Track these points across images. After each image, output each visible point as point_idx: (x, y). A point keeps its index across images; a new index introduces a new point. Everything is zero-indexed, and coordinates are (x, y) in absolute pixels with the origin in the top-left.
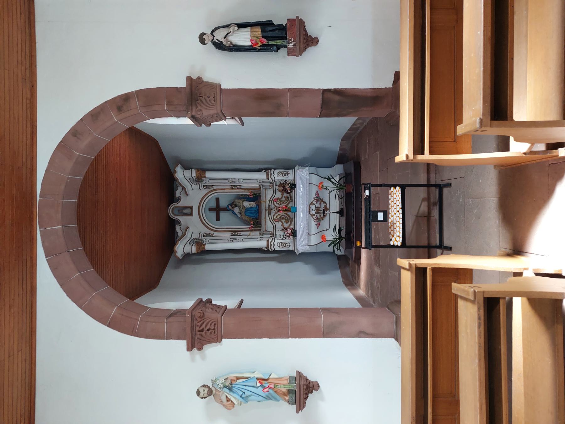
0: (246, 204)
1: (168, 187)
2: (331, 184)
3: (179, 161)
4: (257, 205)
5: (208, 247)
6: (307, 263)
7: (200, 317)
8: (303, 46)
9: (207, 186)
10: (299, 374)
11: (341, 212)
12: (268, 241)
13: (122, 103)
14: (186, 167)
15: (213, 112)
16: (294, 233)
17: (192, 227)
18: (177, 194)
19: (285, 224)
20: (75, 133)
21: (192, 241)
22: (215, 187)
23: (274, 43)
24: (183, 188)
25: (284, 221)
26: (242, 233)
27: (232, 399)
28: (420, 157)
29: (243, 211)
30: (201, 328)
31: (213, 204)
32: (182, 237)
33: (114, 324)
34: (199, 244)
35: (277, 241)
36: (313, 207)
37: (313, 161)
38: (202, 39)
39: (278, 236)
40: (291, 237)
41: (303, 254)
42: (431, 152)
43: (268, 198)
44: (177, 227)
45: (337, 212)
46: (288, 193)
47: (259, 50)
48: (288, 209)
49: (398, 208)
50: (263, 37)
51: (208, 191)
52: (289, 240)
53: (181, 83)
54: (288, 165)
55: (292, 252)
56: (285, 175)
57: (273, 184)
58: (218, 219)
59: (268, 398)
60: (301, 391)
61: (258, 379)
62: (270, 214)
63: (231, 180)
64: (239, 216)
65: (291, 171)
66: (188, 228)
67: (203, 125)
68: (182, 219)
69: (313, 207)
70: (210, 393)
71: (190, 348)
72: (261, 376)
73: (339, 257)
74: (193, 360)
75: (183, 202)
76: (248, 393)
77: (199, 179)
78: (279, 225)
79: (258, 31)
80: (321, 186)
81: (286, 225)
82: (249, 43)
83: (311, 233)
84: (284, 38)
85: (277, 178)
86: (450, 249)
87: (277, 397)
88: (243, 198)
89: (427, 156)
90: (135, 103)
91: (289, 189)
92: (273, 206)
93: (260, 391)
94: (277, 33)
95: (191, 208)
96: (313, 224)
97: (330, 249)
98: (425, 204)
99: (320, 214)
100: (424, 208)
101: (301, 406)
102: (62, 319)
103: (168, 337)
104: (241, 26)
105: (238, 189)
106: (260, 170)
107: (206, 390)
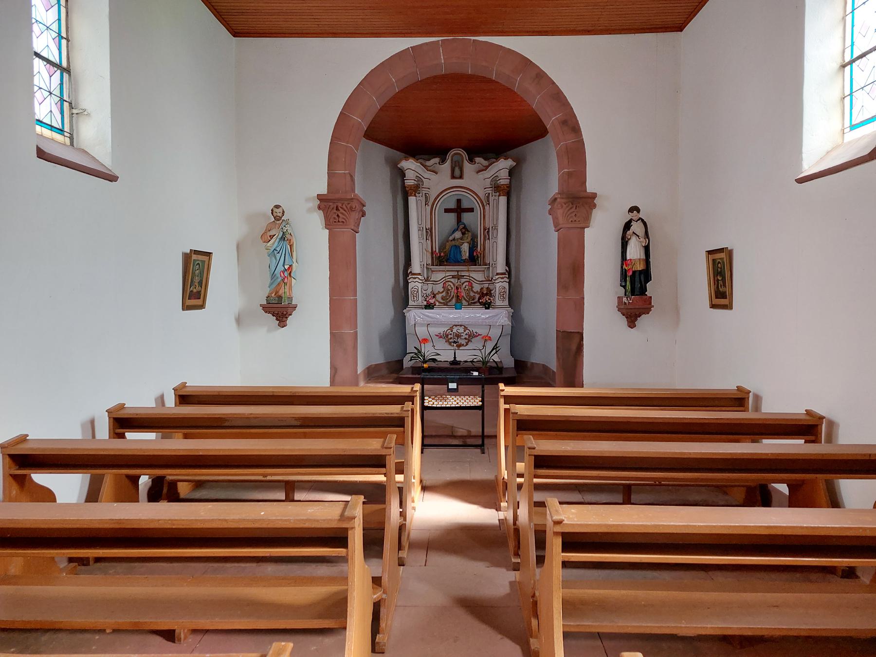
0: (465, 247)
1: (488, 147)
2: (488, 350)
3: (519, 162)
4: (465, 261)
5: (412, 200)
6: (393, 322)
7: (351, 208)
8: (624, 311)
9: (488, 197)
10: (295, 307)
11: (455, 362)
12: (419, 274)
13: (571, 125)
14: (511, 172)
15: (561, 220)
16: (429, 306)
17: (435, 178)
18: (478, 160)
19: (440, 295)
20: (540, 76)
21: (419, 179)
22: (487, 208)
23: (628, 283)
24: (487, 167)
25: (444, 294)
26: (429, 242)
27: (273, 240)
28: (502, 401)
29: (457, 244)
30: (338, 208)
31: (465, 205)
32: (425, 166)
33: (343, 117)
34: (416, 189)
35: (420, 285)
36: (461, 330)
37: (518, 332)
38: (634, 209)
39: (425, 287)
40: (425, 303)
41: (404, 317)
42: (506, 410)
43: (473, 275)
44: (437, 160)
45: (455, 358)
46: (479, 299)
47: (622, 267)
48: (458, 299)
49: (460, 404)
50: (634, 272)
51: (482, 198)
52: (421, 301)
53: (590, 188)
54: (514, 299)
55: (406, 304)
56: (502, 295)
57: (490, 280)
58: (447, 211)
59: (273, 275)
60: (279, 310)
61: (291, 266)
62: (453, 277)
63: (495, 228)
64: (451, 238)
65: (506, 303)
66: (436, 173)
67: (550, 207)
68: (447, 165)
69: (461, 330)
70: (277, 219)
71: (320, 197)
72: (294, 270)
73: (400, 362)
74: (308, 200)
75: (468, 167)
76: (278, 256)
77: (497, 188)
78: (439, 288)
79: (640, 267)
80: (487, 339)
81: (439, 297)
82: (629, 257)
83: (431, 327)
84: (633, 293)
85: (498, 285)
86: (422, 452)
87: (274, 286)
88: (474, 242)
89: (503, 406)
90: (571, 139)
91: (485, 300)
92: (463, 280)
93: (280, 268)
94: (638, 285)
95: (461, 177)
96: (441, 330)
97: (410, 348)
98: (465, 433)
99: (453, 338)
100: (461, 432)
101: (266, 309)
102: (347, 65)
103: (331, 175)
104: (647, 249)
105: (488, 232)
106: (508, 263)
107: (280, 215)
